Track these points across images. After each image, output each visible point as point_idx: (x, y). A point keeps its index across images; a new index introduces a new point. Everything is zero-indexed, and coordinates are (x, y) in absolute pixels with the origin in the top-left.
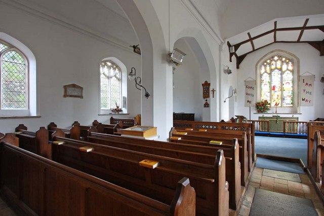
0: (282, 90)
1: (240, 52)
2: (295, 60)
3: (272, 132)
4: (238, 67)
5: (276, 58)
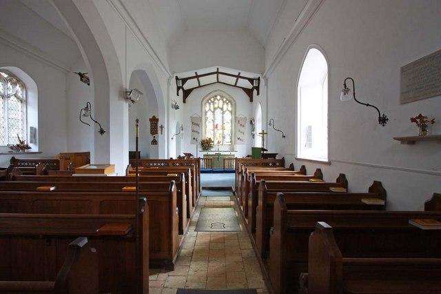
0: (223, 129)
1: (187, 86)
2: (233, 104)
3: (215, 168)
4: (184, 102)
5: (219, 97)
